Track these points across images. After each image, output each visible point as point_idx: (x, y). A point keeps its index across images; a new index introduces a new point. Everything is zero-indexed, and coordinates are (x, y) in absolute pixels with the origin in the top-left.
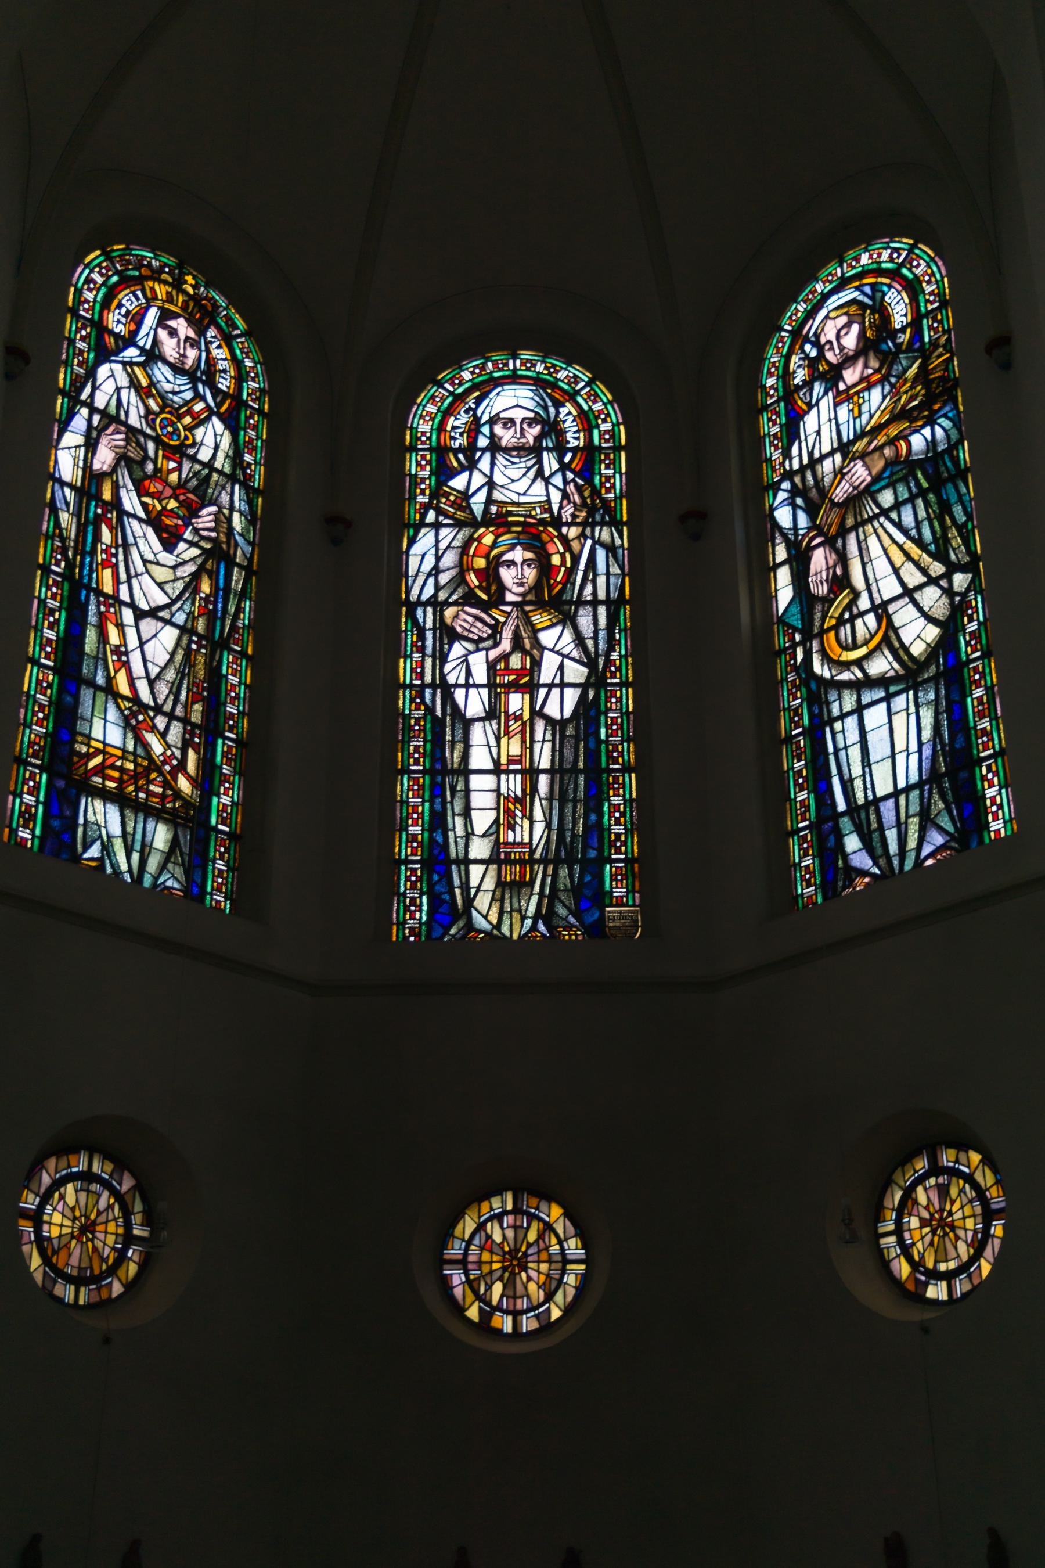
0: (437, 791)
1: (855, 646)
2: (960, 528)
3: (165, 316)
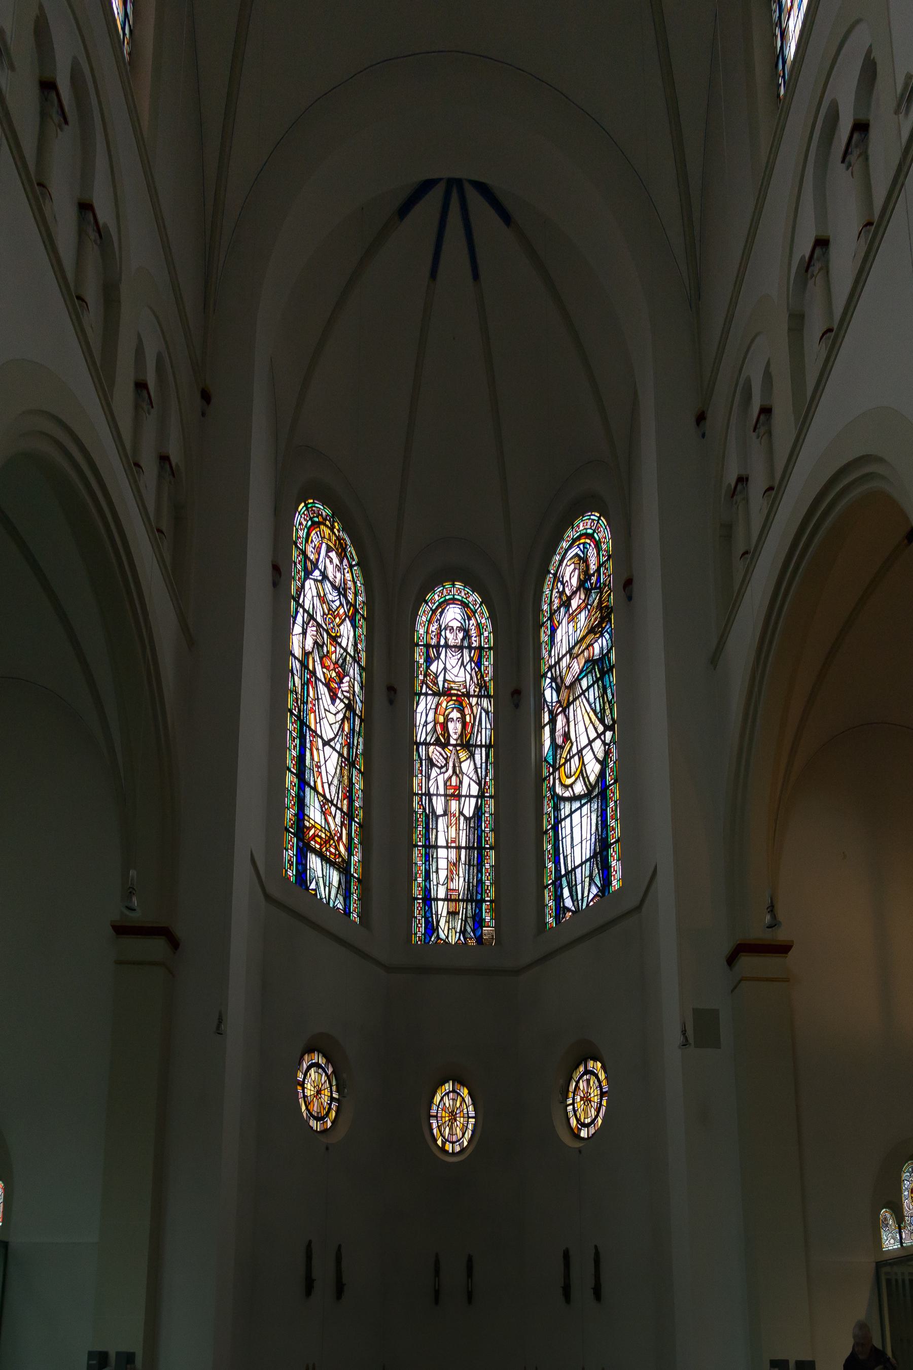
0: (427, 859)
1: (571, 776)
2: (610, 702)
3: (329, 549)
